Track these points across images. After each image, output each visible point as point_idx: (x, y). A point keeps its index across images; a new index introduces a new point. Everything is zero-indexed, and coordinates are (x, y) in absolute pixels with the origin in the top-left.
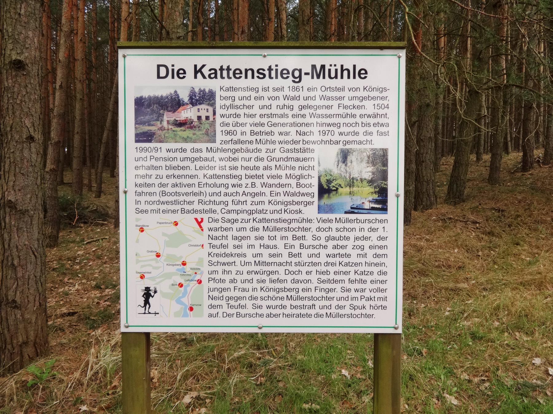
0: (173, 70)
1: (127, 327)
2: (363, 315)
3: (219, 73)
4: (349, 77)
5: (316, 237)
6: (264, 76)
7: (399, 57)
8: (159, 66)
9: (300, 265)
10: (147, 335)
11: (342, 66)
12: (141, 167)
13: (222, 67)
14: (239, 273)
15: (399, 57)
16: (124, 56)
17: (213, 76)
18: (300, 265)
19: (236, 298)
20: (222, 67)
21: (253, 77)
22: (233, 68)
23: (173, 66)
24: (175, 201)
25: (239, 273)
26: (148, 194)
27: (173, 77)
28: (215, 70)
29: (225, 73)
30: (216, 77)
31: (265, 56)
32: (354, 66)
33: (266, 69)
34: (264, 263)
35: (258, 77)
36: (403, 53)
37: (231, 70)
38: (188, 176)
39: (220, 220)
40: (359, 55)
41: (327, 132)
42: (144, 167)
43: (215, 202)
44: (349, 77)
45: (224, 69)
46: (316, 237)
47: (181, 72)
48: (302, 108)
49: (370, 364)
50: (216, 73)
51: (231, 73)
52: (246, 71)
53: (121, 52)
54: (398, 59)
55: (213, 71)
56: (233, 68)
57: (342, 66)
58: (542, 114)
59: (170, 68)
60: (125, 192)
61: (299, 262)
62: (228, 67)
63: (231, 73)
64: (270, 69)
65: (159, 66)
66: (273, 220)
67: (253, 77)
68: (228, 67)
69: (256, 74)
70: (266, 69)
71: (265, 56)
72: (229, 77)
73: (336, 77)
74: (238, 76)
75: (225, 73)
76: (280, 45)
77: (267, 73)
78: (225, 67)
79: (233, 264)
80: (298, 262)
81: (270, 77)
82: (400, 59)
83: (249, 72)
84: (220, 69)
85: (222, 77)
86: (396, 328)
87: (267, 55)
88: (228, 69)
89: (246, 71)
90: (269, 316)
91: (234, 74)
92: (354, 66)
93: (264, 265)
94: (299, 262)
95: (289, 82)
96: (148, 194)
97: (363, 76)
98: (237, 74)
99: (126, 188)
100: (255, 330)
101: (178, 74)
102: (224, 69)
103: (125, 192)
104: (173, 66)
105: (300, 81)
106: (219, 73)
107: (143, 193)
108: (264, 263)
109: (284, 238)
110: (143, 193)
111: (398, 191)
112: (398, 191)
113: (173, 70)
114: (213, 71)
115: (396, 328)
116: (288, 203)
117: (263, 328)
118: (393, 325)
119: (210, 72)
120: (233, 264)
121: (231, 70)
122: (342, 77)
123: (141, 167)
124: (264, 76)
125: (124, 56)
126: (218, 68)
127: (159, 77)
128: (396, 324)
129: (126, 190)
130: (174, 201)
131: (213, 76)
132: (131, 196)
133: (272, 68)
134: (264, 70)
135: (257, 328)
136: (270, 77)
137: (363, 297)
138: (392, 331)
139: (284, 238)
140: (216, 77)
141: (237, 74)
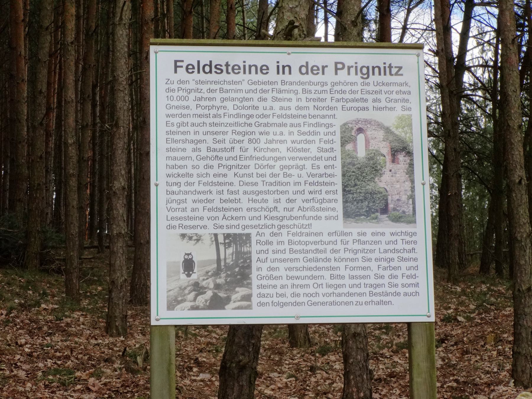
1: (157, 320)
4: (380, 74)
6: (222, 71)
10: (409, 324)
16: (156, 53)
19: (335, 286)
22: (231, 64)
31: (289, 54)
32: (199, 62)
33: (223, 65)
35: (216, 72)
37: (229, 65)
44: (380, 74)
48: (224, 100)
49: (407, 355)
52: (373, 68)
53: (152, 48)
54: (417, 57)
56: (231, 64)
60: (157, 185)
62: (390, 65)
64: (227, 65)
68: (390, 65)
70: (223, 65)
71: (289, 54)
74: (236, 71)
76: (350, 45)
77: (224, 68)
83: (248, 69)
84: (225, 65)
86: (429, 317)
88: (390, 67)
89: (373, 68)
91: (233, 69)
92: (199, 62)
95: (357, 79)
97: (264, 72)
98: (236, 69)
101: (312, 70)
103: (157, 185)
104: (244, 62)
105: (368, 77)
111: (157, 181)
112: (157, 181)
115: (429, 317)
117: (161, 320)
118: (425, 312)
121: (229, 65)
124: (222, 71)
125: (156, 53)
129: (157, 182)
134: (221, 66)
135: (426, 317)
136: (228, 73)
141: (236, 69)
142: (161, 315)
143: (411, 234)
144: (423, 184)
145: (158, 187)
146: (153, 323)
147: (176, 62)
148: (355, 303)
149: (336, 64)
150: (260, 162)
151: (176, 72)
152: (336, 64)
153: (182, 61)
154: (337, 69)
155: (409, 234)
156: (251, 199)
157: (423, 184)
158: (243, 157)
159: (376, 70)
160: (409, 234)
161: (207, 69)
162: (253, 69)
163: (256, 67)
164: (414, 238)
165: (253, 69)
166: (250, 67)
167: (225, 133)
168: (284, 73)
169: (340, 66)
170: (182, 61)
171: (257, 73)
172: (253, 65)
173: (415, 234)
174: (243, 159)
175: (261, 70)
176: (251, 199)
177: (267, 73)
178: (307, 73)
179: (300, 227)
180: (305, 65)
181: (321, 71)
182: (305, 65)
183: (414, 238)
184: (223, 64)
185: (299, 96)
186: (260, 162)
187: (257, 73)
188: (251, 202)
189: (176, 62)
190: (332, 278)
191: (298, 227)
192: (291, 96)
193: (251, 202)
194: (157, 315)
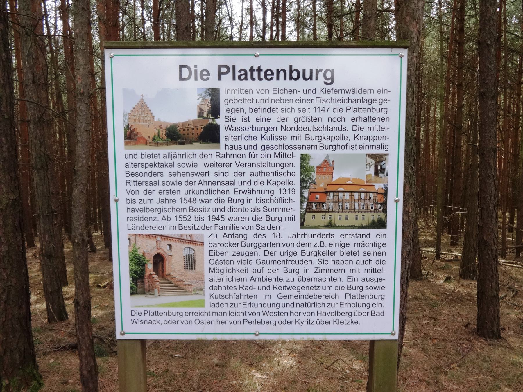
0: (196, 71)
2: (206, 313)
3: (249, 74)
4: (285, 79)
7: (401, 57)
8: (181, 67)
9: (271, 166)
11: (291, 67)
12: (358, 119)
13: (252, 67)
14: (289, 280)
15: (401, 57)
16: (111, 57)
17: (243, 77)
20: (252, 67)
23: (196, 66)
25: (289, 280)
26: (171, 201)
27: (196, 79)
28: (245, 71)
29: (256, 74)
30: (246, 78)
31: (257, 56)
34: (375, 270)
37: (262, 70)
38: (210, 183)
39: (255, 227)
40: (380, 55)
42: (361, 119)
43: (271, 164)
45: (254, 70)
47: (205, 73)
50: (246, 74)
51: (262, 74)
52: (278, 71)
54: (400, 58)
55: (243, 72)
57: (291, 67)
58: (502, 113)
59: (193, 69)
60: (117, 201)
62: (259, 67)
63: (262, 74)
65: (181, 67)
68: (259, 67)
71: (257, 56)
72: (260, 79)
73: (311, 78)
74: (269, 77)
75: (256, 74)
78: (256, 68)
79: (207, 174)
82: (403, 58)
85: (253, 79)
87: (260, 55)
88: (259, 70)
89: (278, 71)
90: (321, 322)
91: (266, 75)
93: (375, 271)
96: (171, 201)
98: (268, 75)
99: (397, 197)
100: (252, 337)
102: (254, 70)
103: (117, 201)
106: (249, 74)
107: (167, 201)
108: (375, 270)
110: (167, 201)
112: (397, 197)
113: (196, 71)
114: (243, 72)
117: (260, 335)
120: (207, 174)
121: (262, 70)
122: (311, 71)
123: (358, 119)
126: (248, 69)
127: (181, 79)
128: (393, 330)
129: (117, 198)
131: (243, 77)
132: (122, 204)
135: (254, 335)
137: (348, 295)
140: (246, 78)
141: (268, 75)
142: (126, 330)
143: (380, 245)
144: (397, 201)
145: (118, 203)
146: (118, 337)
148: (326, 305)
149: (220, 67)
151: (220, 79)
152: (220, 67)
154: (220, 74)
155: (377, 245)
156: (319, 312)
158: (352, 278)
159: (282, 74)
160: (377, 245)
164: (382, 249)
167: (228, 165)
168: (311, 71)
169: (224, 70)
173: (384, 245)
174: (351, 280)
176: (319, 312)
177: (208, 79)
181: (275, 76)
183: (382, 249)
188: (319, 315)
190: (286, 271)
193: (319, 315)
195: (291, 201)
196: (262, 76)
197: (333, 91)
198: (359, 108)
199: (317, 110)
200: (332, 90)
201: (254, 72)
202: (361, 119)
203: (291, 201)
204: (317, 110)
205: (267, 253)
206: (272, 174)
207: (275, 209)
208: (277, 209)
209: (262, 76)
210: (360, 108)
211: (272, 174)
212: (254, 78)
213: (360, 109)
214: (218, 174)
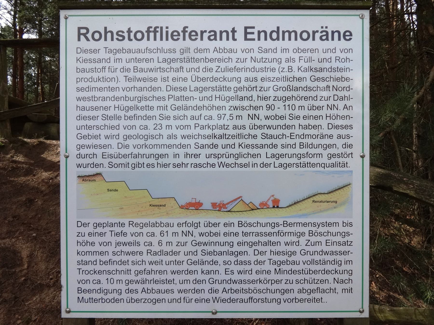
0: (167, 32)
5: (113, 164)
11: (106, 28)
12: (133, 89)
15: (362, 18)
16: (66, 18)
17: (212, 38)
18: (304, 273)
21: (112, 39)
24: (92, 97)
33: (125, 31)
35: (117, 39)
36: (366, 13)
37: (132, 32)
41: (223, 116)
42: (136, 89)
44: (161, 39)
46: (113, 164)
52: (221, 32)
55: (212, 33)
57: (106, 28)
60: (67, 157)
61: (303, 270)
64: (129, 31)
66: (310, 224)
67: (112, 39)
69: (115, 36)
70: (125, 31)
77: (126, 35)
80: (301, 270)
81: (130, 40)
84: (182, 31)
89: (221, 32)
94: (303, 270)
97: (348, 38)
99: (66, 152)
101: (172, 35)
109: (348, 262)
112: (66, 152)
113: (167, 32)
114: (212, 33)
115: (361, 312)
116: (346, 234)
118: (358, 307)
119: (210, 34)
121: (132, 32)
123: (133, 89)
125: (66, 18)
130: (91, 96)
133: (131, 30)
134: (123, 32)
136: (130, 40)
138: (357, 315)
139: (348, 262)
144: (363, 157)
146: (64, 315)
147: (246, 28)
149: (79, 29)
150: (114, 161)
152: (79, 29)
153: (253, 28)
157: (363, 157)
158: (107, 154)
161: (274, 35)
162: (336, 35)
163: (265, 32)
165: (336, 35)
166: (333, 33)
170: (253, 28)
171: (339, 39)
172: (337, 31)
175: (344, 36)
177: (350, 39)
178: (278, 39)
179: (311, 282)
180: (276, 30)
181: (199, 37)
182: (276, 30)
184: (125, 30)
185: (282, 65)
186: (114, 161)
187: (266, 39)
189: (246, 28)
191: (308, 282)
192: (275, 65)
194: (67, 308)
195: (284, 136)
196: (132, 36)
197: (236, 69)
198: (181, 97)
199: (287, 108)
200: (235, 68)
201: (150, 33)
202: (136, 89)
203: (284, 136)
204: (287, 108)
205: (256, 252)
206: (106, 89)
207: (156, 146)
208: (158, 146)
209: (132, 36)
210: (182, 96)
211: (106, 89)
212: (235, 38)
213: (182, 98)
214: (285, 146)
